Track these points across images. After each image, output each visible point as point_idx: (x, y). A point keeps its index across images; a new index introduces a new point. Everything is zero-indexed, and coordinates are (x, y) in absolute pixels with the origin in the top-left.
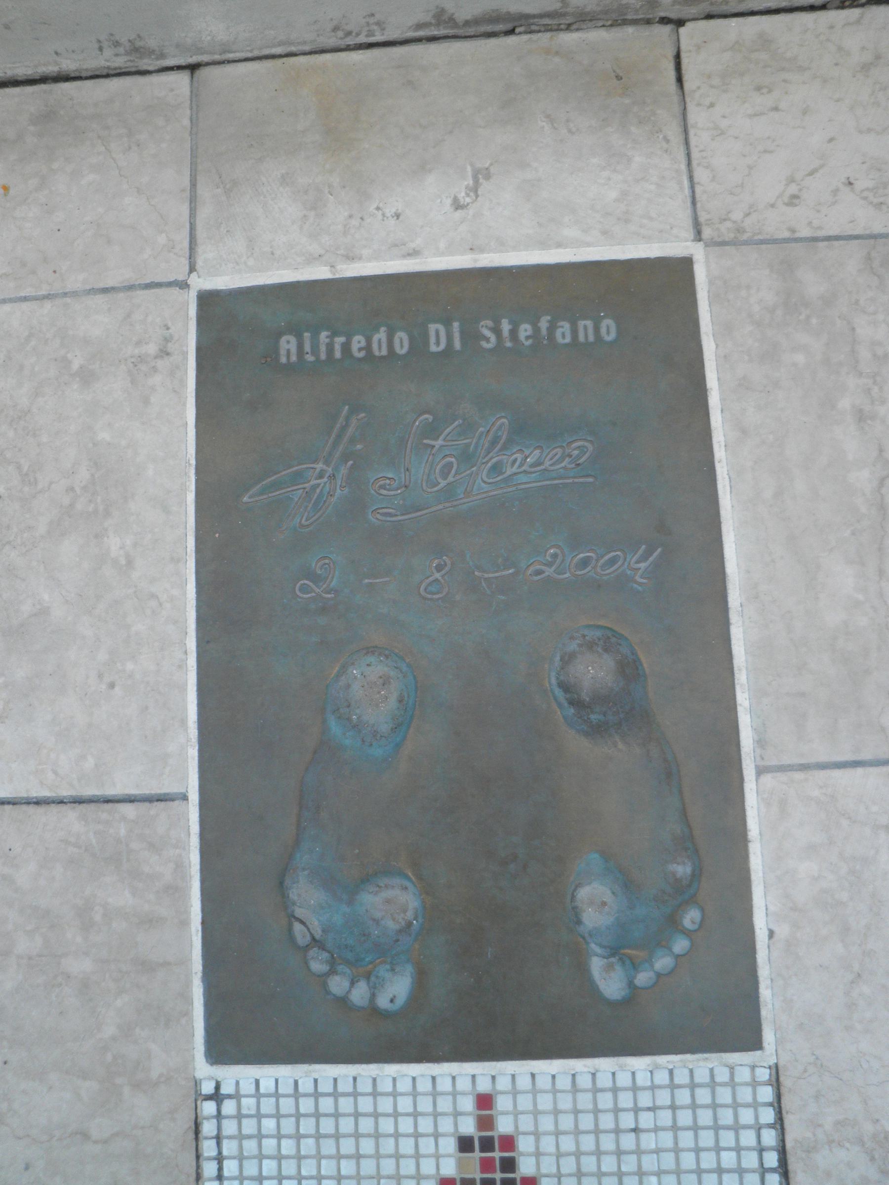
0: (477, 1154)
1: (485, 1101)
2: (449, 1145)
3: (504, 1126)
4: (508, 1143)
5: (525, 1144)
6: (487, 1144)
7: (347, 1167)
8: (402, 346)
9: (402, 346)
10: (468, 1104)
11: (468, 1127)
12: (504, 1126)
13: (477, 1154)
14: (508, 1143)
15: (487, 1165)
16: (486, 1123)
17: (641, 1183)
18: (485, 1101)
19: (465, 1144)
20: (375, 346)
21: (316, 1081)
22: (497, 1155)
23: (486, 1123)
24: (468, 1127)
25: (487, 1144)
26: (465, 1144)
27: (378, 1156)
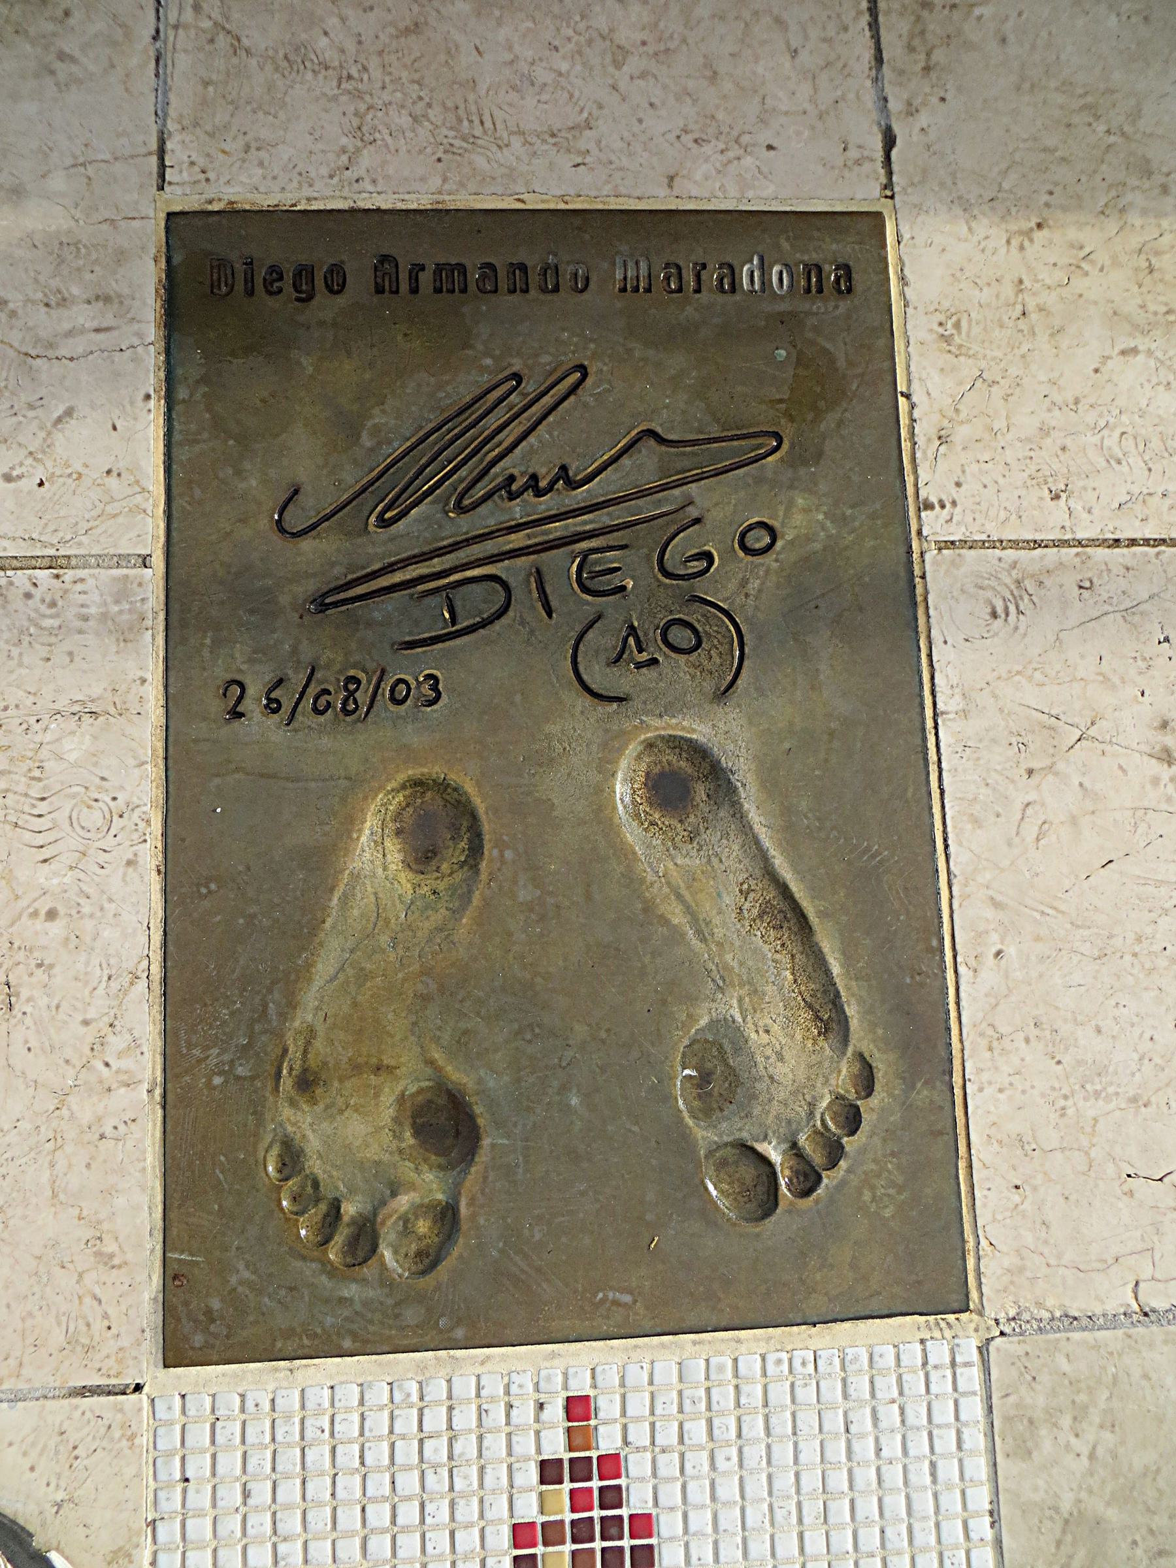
3: (607, 1442)
4: (611, 1464)
5: (637, 1465)
12: (607, 1442)
14: (611, 1464)
15: (578, 1500)
16: (577, 1438)
19: (549, 1471)
24: (556, 1447)
26: (549, 1471)
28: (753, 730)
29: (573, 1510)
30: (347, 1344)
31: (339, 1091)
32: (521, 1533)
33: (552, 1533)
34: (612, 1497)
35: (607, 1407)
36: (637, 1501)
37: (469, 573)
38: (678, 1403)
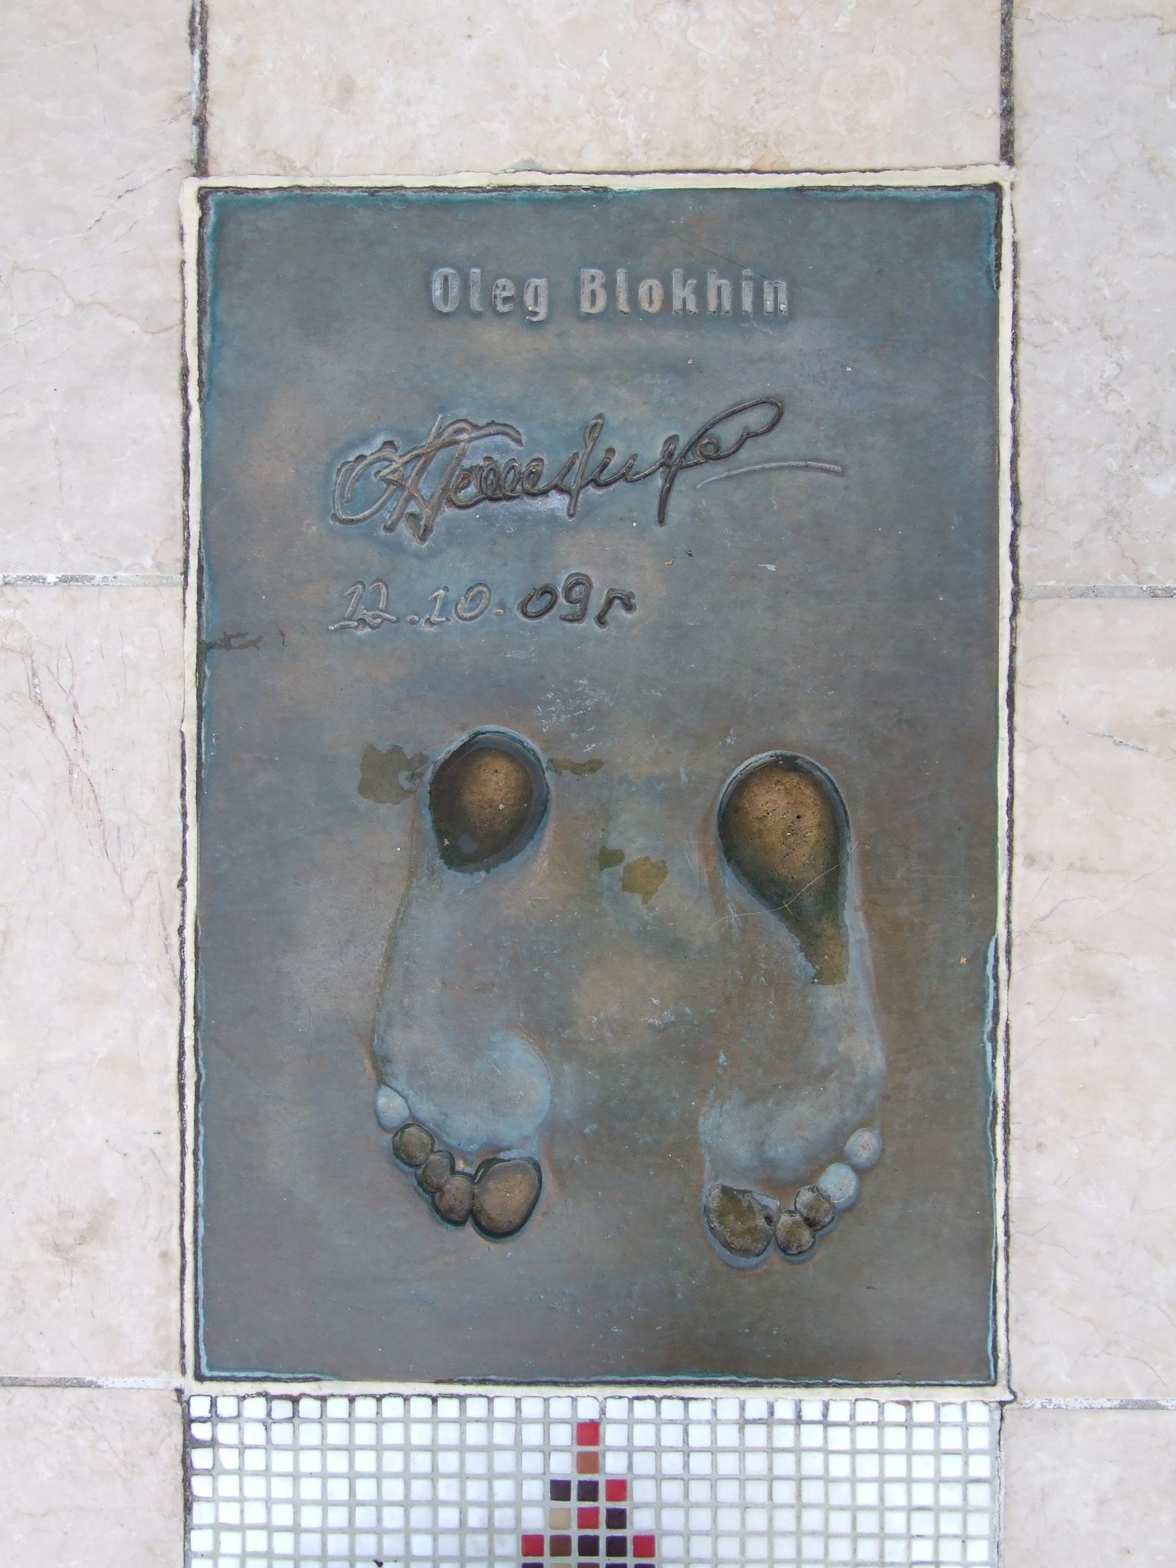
0: (574, 1504)
1: (589, 1432)
2: (536, 1490)
3: (613, 1465)
4: (618, 1489)
5: (641, 1491)
6: (589, 1491)
7: (284, 1543)
8: (651, 302)
9: (651, 302)
10: (563, 1435)
11: (563, 1466)
12: (613, 1465)
13: (574, 1504)
14: (618, 1489)
15: (587, 1518)
16: (589, 1462)
17: (216, 1565)
18: (589, 1432)
19: (560, 1490)
20: (529, 299)
21: (662, 520)
22: (603, 1504)
23: (589, 1462)
24: (563, 1466)
25: (589, 1491)
26: (560, 1490)
27: (771, 1451)
28: (698, 943)
29: (568, 1498)
30: (205, 390)
31: (546, 1450)
32: (532, 1544)
33: (561, 1546)
34: (617, 1519)
35: (612, 1435)
36: (640, 1522)
37: (767, 466)
38: (681, 1445)
